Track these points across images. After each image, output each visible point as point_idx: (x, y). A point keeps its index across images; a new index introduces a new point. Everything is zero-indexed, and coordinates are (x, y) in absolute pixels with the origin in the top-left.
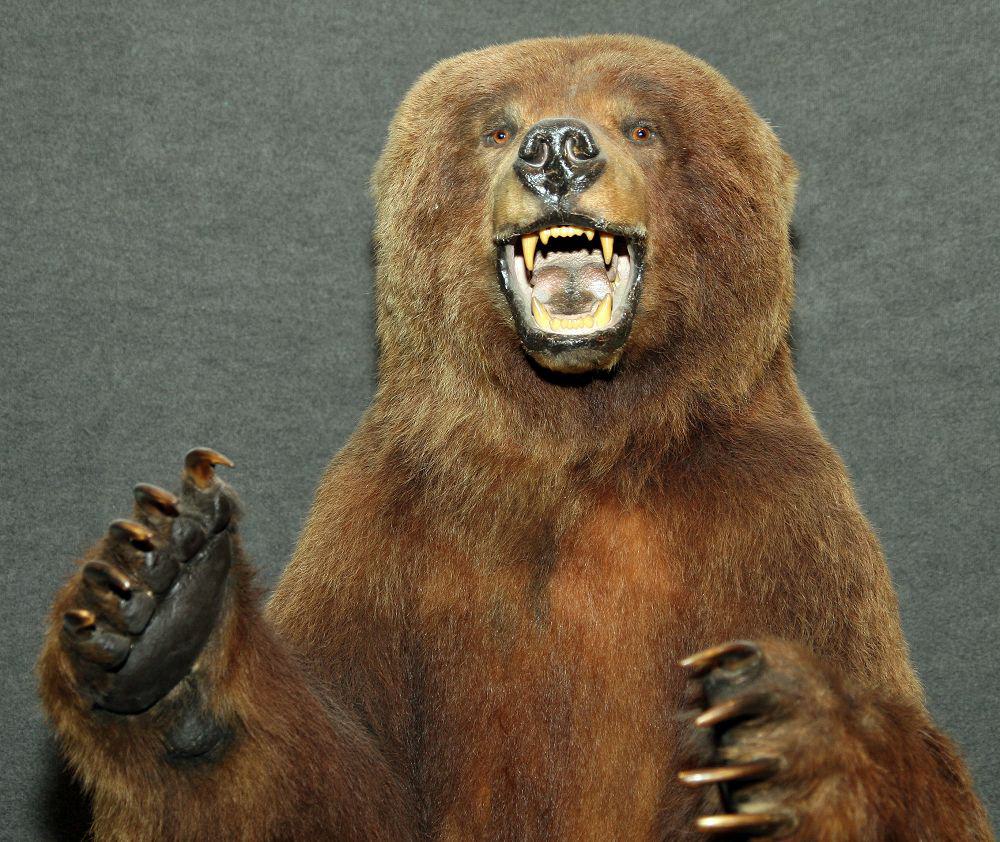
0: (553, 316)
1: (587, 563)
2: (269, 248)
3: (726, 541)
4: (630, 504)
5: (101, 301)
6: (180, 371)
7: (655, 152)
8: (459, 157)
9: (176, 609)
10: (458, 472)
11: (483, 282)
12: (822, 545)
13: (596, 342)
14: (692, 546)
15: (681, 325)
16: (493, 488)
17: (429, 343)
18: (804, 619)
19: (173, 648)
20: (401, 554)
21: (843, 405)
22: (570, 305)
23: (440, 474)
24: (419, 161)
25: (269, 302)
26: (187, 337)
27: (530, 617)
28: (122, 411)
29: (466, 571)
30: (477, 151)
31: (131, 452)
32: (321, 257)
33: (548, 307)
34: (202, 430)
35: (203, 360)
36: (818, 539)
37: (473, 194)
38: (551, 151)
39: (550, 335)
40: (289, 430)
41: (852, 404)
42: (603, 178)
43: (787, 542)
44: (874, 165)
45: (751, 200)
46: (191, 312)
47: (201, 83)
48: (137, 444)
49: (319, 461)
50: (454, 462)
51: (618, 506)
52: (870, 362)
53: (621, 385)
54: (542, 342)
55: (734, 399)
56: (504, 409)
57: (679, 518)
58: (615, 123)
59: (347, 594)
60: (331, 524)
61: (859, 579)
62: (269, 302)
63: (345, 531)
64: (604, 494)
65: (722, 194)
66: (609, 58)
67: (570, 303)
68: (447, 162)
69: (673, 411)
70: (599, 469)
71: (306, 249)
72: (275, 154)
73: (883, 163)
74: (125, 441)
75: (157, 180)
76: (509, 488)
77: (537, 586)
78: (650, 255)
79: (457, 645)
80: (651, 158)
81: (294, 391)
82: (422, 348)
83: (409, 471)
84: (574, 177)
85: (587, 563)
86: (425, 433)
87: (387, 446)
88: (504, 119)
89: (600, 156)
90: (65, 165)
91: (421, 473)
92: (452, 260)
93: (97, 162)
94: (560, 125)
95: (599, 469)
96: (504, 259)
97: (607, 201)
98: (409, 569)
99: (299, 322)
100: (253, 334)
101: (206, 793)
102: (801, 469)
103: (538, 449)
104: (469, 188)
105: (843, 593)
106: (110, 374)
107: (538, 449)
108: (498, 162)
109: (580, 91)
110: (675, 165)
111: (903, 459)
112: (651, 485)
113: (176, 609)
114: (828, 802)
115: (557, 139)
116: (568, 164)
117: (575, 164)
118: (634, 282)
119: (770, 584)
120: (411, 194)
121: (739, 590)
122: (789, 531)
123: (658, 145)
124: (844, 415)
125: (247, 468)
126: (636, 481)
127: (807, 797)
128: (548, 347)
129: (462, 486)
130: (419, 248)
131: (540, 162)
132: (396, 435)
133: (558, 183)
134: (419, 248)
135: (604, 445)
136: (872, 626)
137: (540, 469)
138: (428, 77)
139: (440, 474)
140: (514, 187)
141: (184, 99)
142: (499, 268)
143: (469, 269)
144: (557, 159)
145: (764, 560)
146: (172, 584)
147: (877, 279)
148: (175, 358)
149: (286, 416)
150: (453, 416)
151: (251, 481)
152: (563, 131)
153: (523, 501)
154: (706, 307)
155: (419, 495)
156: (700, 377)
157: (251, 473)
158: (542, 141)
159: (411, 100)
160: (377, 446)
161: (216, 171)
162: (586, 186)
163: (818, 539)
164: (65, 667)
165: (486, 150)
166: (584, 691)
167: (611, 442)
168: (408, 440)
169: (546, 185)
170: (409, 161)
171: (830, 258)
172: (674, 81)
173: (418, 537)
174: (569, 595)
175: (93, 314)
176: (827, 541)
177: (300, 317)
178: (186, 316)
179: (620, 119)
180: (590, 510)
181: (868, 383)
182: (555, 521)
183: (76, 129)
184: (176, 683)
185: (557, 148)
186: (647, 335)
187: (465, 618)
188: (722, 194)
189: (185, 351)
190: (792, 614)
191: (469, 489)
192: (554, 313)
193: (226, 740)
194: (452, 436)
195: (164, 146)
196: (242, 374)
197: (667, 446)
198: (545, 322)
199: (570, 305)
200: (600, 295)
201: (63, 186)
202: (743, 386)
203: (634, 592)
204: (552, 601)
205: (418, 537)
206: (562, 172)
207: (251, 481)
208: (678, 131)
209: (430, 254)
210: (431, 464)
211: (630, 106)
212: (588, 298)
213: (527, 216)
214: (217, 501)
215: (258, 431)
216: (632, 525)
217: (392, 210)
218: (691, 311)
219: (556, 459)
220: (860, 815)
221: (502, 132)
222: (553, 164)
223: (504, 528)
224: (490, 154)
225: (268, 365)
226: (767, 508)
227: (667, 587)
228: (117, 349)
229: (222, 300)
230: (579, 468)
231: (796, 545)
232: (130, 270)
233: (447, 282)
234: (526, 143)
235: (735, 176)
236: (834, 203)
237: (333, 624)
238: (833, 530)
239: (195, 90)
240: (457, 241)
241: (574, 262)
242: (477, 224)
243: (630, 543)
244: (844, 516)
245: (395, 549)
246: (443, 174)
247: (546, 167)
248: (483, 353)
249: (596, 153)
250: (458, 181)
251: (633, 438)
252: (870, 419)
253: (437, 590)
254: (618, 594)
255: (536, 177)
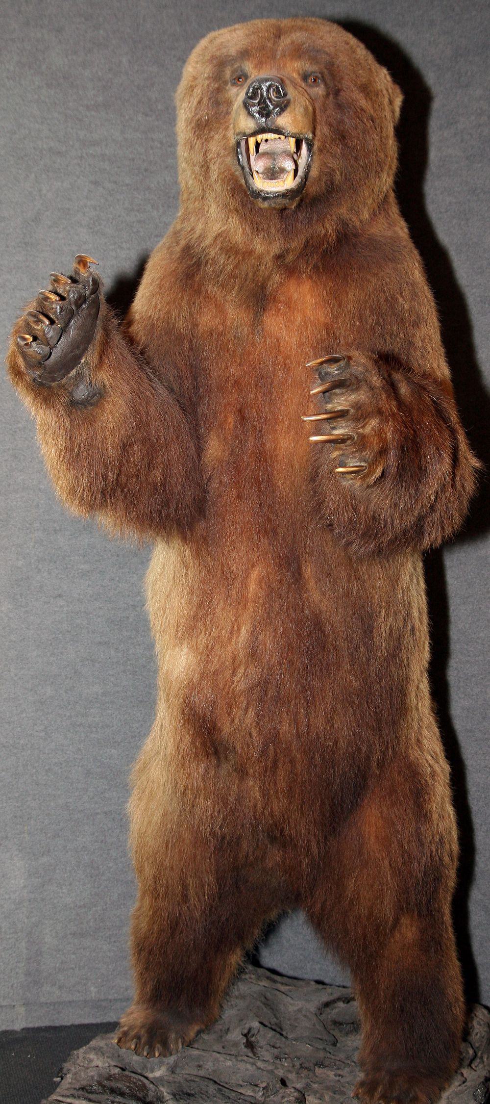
0: (264, 180)
1: (282, 307)
2: (127, 117)
3: (353, 296)
4: (305, 276)
5: (34, 148)
6: (78, 188)
7: (319, 90)
8: (219, 90)
9: (72, 332)
10: (218, 258)
11: (229, 160)
12: (401, 300)
13: (285, 195)
14: (336, 299)
15: (332, 184)
16: (236, 267)
17: (203, 190)
18: (388, 338)
19: (72, 352)
20: (189, 301)
21: (441, 212)
22: (273, 175)
23: (209, 259)
24: (198, 91)
25: (127, 149)
26: (83, 169)
27: (253, 334)
28: (48, 211)
29: (220, 309)
30: (227, 88)
31: (53, 234)
32: (156, 123)
33: (261, 176)
34: (92, 222)
35: (91, 182)
36: (398, 296)
37: (225, 112)
38: (262, 95)
39: (261, 191)
40: (139, 222)
41: (446, 212)
42: (289, 109)
43: (383, 298)
44: (464, 75)
45: (371, 116)
46: (84, 155)
47: (86, 20)
48: (56, 229)
49: (155, 239)
50: (216, 253)
51: (299, 278)
52: (456, 189)
53: (301, 215)
54: (257, 194)
55: (361, 222)
56: (242, 226)
57: (330, 284)
58: (299, 74)
59: (161, 321)
60: (154, 284)
61: (418, 317)
62: (127, 149)
63: (160, 288)
64: (291, 271)
65: (356, 113)
66: (298, 36)
67: (273, 174)
68: (213, 92)
69: (328, 228)
70: (290, 258)
71: (148, 118)
72: (130, 62)
73: (469, 74)
74: (50, 227)
75: (64, 77)
76: (244, 268)
77: (257, 319)
78: (315, 147)
79: (216, 347)
80: (318, 93)
81: (142, 200)
82: (200, 192)
83: (194, 257)
84: (274, 109)
85: (282, 307)
86: (202, 237)
87: (183, 243)
88: (241, 71)
89: (288, 97)
90: (12, 68)
91: (200, 258)
92: (214, 147)
93: (30, 67)
94: (267, 80)
95: (290, 258)
96: (240, 149)
97: (291, 122)
98: (193, 309)
99: (144, 161)
100: (119, 167)
101: (90, 421)
102: (394, 260)
103: (259, 246)
104: (223, 108)
105: (409, 325)
106: (40, 190)
107: (259, 246)
108: (237, 95)
109: (282, 57)
110: (331, 97)
111: (471, 244)
112: (316, 267)
113: (72, 332)
114: (373, 429)
115: (264, 88)
116: (271, 102)
117: (274, 101)
118: (308, 161)
119: (372, 319)
120: (194, 109)
121: (358, 323)
122: (384, 292)
123: (322, 86)
124: (441, 218)
125: (116, 243)
126: (308, 264)
127: (363, 427)
128: (261, 198)
129: (220, 266)
130: (198, 139)
131: (256, 100)
132: (187, 238)
133: (265, 113)
134: (198, 139)
135: (293, 245)
136: (423, 341)
137: (260, 257)
138: (203, 42)
139: (209, 259)
140: (243, 112)
141: (77, 29)
142: (237, 154)
143: (222, 153)
144: (265, 99)
145: (371, 307)
146: (69, 321)
147: (462, 141)
148: (75, 181)
149: (138, 214)
150: (216, 228)
151: (118, 251)
152: (268, 84)
153: (251, 274)
154: (346, 174)
155: (199, 270)
156: (343, 211)
157: (119, 246)
158: (257, 89)
159: (194, 56)
160: (178, 243)
161: (97, 72)
162: (280, 114)
163: (398, 296)
164: (20, 361)
165: (232, 88)
166: (280, 370)
167: (296, 244)
168: (193, 241)
169: (259, 113)
170: (193, 91)
171: (438, 128)
172: (332, 50)
173: (198, 292)
174: (273, 323)
175: (30, 156)
176: (403, 298)
177: (145, 158)
178: (81, 157)
179: (301, 72)
180: (284, 280)
181: (455, 201)
182: (267, 285)
183: (18, 47)
184: (73, 369)
185: (265, 93)
186: (312, 189)
187: (220, 334)
188: (356, 113)
189: (81, 177)
190: (382, 336)
191: (224, 267)
192: (264, 179)
193: (98, 397)
194: (215, 239)
195: (67, 57)
196: (113, 190)
197: (325, 246)
198: (260, 183)
199: (273, 175)
200: (288, 169)
201: (11, 82)
202: (366, 215)
203: (305, 322)
204: (265, 326)
205: (198, 292)
206: (267, 106)
207: (118, 251)
208: (333, 76)
209: (203, 143)
210: (205, 253)
211: (307, 66)
212: (283, 170)
213: (249, 129)
214: (91, 280)
215: (122, 222)
216: (306, 287)
217: (184, 117)
218: (338, 177)
219: (268, 252)
220: (389, 436)
221: (240, 78)
222: (263, 102)
223: (241, 289)
224: (233, 90)
225: (127, 185)
226: (374, 280)
227: (322, 319)
228: (44, 176)
229: (101, 148)
230: (279, 257)
231: (387, 299)
232: (50, 130)
233: (212, 159)
234: (249, 90)
235: (363, 102)
236: (441, 97)
237: (154, 336)
238: (407, 292)
239: (84, 23)
240: (216, 137)
241: (277, 149)
242: (227, 128)
243: (305, 297)
244: (413, 285)
245: (186, 298)
246: (210, 99)
247: (259, 103)
248: (230, 197)
249: (286, 95)
250: (217, 103)
251: (307, 242)
252: (455, 221)
253: (207, 320)
254: (298, 322)
255: (254, 108)
